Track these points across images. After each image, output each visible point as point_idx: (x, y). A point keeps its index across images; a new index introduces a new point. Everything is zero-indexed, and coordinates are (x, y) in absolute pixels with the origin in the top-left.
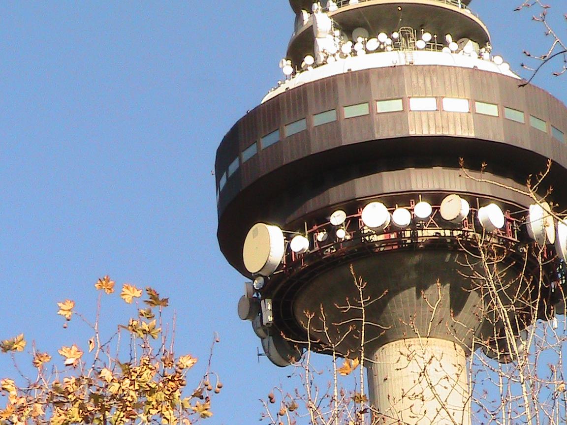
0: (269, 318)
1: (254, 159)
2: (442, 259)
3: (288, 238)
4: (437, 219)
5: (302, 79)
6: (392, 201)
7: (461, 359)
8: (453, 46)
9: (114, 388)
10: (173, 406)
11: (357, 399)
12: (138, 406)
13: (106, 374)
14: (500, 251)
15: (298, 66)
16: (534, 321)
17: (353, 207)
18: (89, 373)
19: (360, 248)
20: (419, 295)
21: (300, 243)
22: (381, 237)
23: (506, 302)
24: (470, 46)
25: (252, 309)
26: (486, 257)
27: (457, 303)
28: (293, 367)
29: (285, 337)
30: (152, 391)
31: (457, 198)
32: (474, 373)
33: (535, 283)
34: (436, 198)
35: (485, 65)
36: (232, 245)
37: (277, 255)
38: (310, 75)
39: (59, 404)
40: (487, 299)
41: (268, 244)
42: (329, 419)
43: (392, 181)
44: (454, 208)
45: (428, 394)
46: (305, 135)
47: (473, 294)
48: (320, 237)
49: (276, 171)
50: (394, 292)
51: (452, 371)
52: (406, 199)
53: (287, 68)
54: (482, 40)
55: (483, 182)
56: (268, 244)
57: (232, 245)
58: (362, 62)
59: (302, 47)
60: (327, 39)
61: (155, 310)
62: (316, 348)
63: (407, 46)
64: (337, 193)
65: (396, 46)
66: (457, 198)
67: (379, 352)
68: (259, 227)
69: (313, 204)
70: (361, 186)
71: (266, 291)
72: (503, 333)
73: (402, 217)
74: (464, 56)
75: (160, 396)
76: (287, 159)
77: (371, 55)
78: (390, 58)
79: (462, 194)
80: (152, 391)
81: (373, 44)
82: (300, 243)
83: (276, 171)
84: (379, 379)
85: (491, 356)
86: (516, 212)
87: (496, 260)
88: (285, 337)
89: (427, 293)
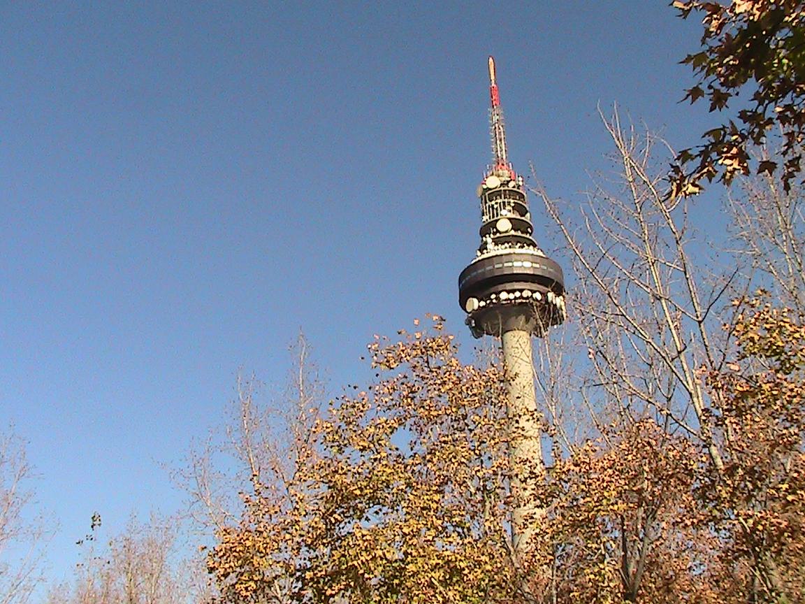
0: (474, 325)
1: (475, 276)
2: (524, 308)
3: (479, 302)
4: (521, 297)
5: (483, 256)
6: (509, 292)
7: (528, 337)
8: (526, 247)
9: (430, 345)
10: (447, 350)
11: (499, 348)
12: (437, 350)
13: (428, 341)
14: (540, 306)
15: (482, 253)
16: (550, 326)
17: (498, 293)
18: (423, 341)
19: (499, 305)
20: (517, 318)
21: (482, 304)
22: (506, 302)
23: (542, 321)
24: (531, 247)
25: (469, 323)
26: (555, 572)
27: (527, 321)
28: (480, 339)
29: (478, 331)
30: (441, 346)
31: (527, 291)
32: (532, 341)
33: (550, 316)
34: (521, 291)
35: (536, 253)
36: (463, 305)
37: (476, 307)
38: (486, 256)
39: (415, 349)
40: (536, 320)
41: (474, 304)
42: (539, 192)
43: (509, 286)
44: (526, 294)
45: (519, 347)
46: (484, 273)
47: (532, 318)
48: (488, 302)
49: (477, 282)
50: (510, 317)
51: (526, 341)
52: (513, 291)
53: (479, 253)
54: (535, 246)
55: (535, 286)
56: (474, 304)
57: (463, 305)
58: (499, 253)
59: (483, 247)
60: (490, 246)
61: (443, 322)
62: (487, 334)
63: (373, 436)
64: (492, 290)
65: (510, 247)
66: (527, 291)
67: (505, 335)
68: (471, 299)
69: (487, 292)
70: (500, 287)
71: (472, 318)
72: (540, 330)
73: (511, 296)
74: (530, 250)
75: (443, 347)
76: (479, 279)
77: (502, 250)
78: (508, 251)
79: (529, 290)
80: (441, 346)
81: (503, 247)
82: (482, 304)
83: (477, 282)
84: (504, 343)
85: (537, 336)
86: (544, 294)
87: (539, 309)
88: (478, 331)
89: (519, 318)
